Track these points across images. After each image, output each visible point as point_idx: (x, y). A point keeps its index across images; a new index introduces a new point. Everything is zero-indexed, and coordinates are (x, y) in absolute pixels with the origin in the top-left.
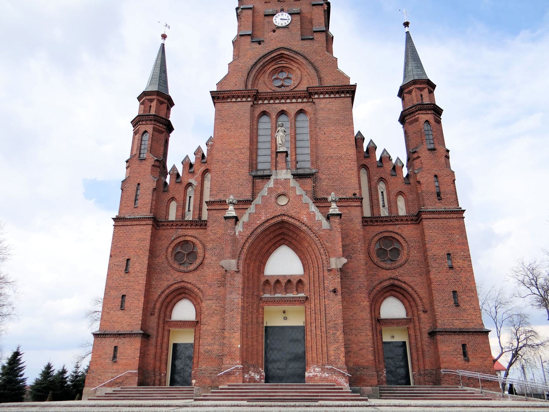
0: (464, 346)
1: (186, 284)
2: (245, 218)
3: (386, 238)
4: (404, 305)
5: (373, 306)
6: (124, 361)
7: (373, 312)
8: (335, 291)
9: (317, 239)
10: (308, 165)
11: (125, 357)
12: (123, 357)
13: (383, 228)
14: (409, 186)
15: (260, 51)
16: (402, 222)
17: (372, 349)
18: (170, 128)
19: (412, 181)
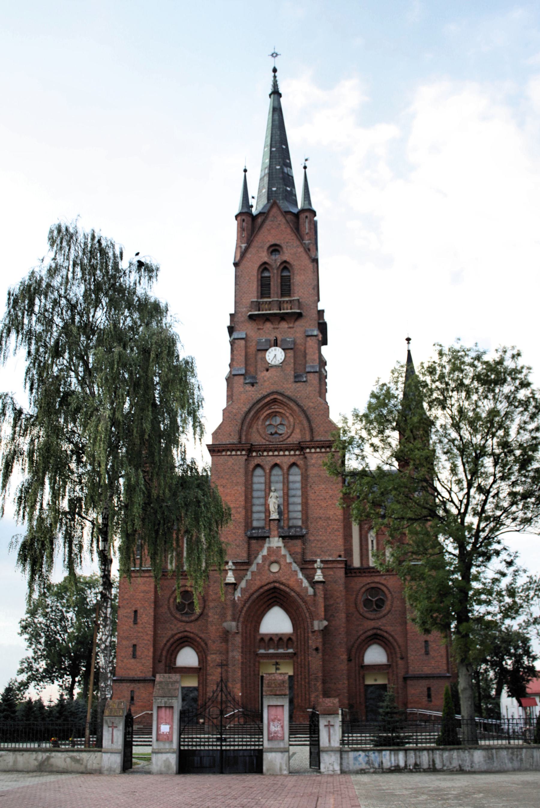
1: (188, 634)
2: (243, 584)
6: (140, 704)
8: (317, 649)
10: (299, 523)
13: (370, 579)
15: (254, 394)
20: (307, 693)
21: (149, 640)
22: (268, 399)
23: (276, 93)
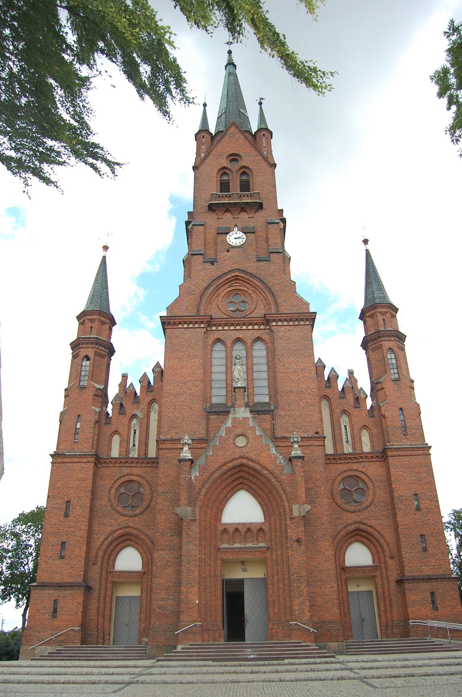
0: (432, 594)
1: (131, 530)
2: (201, 461)
3: (350, 477)
4: (371, 551)
5: (337, 553)
7: (337, 560)
8: (298, 541)
9: (279, 484)
11: (66, 613)
12: (64, 613)
14: (373, 419)
15: (212, 271)
16: (367, 460)
17: (338, 601)
18: (111, 351)
19: (376, 413)
20: (287, 599)
21: (81, 537)
22: (229, 276)
23: (231, 64)
